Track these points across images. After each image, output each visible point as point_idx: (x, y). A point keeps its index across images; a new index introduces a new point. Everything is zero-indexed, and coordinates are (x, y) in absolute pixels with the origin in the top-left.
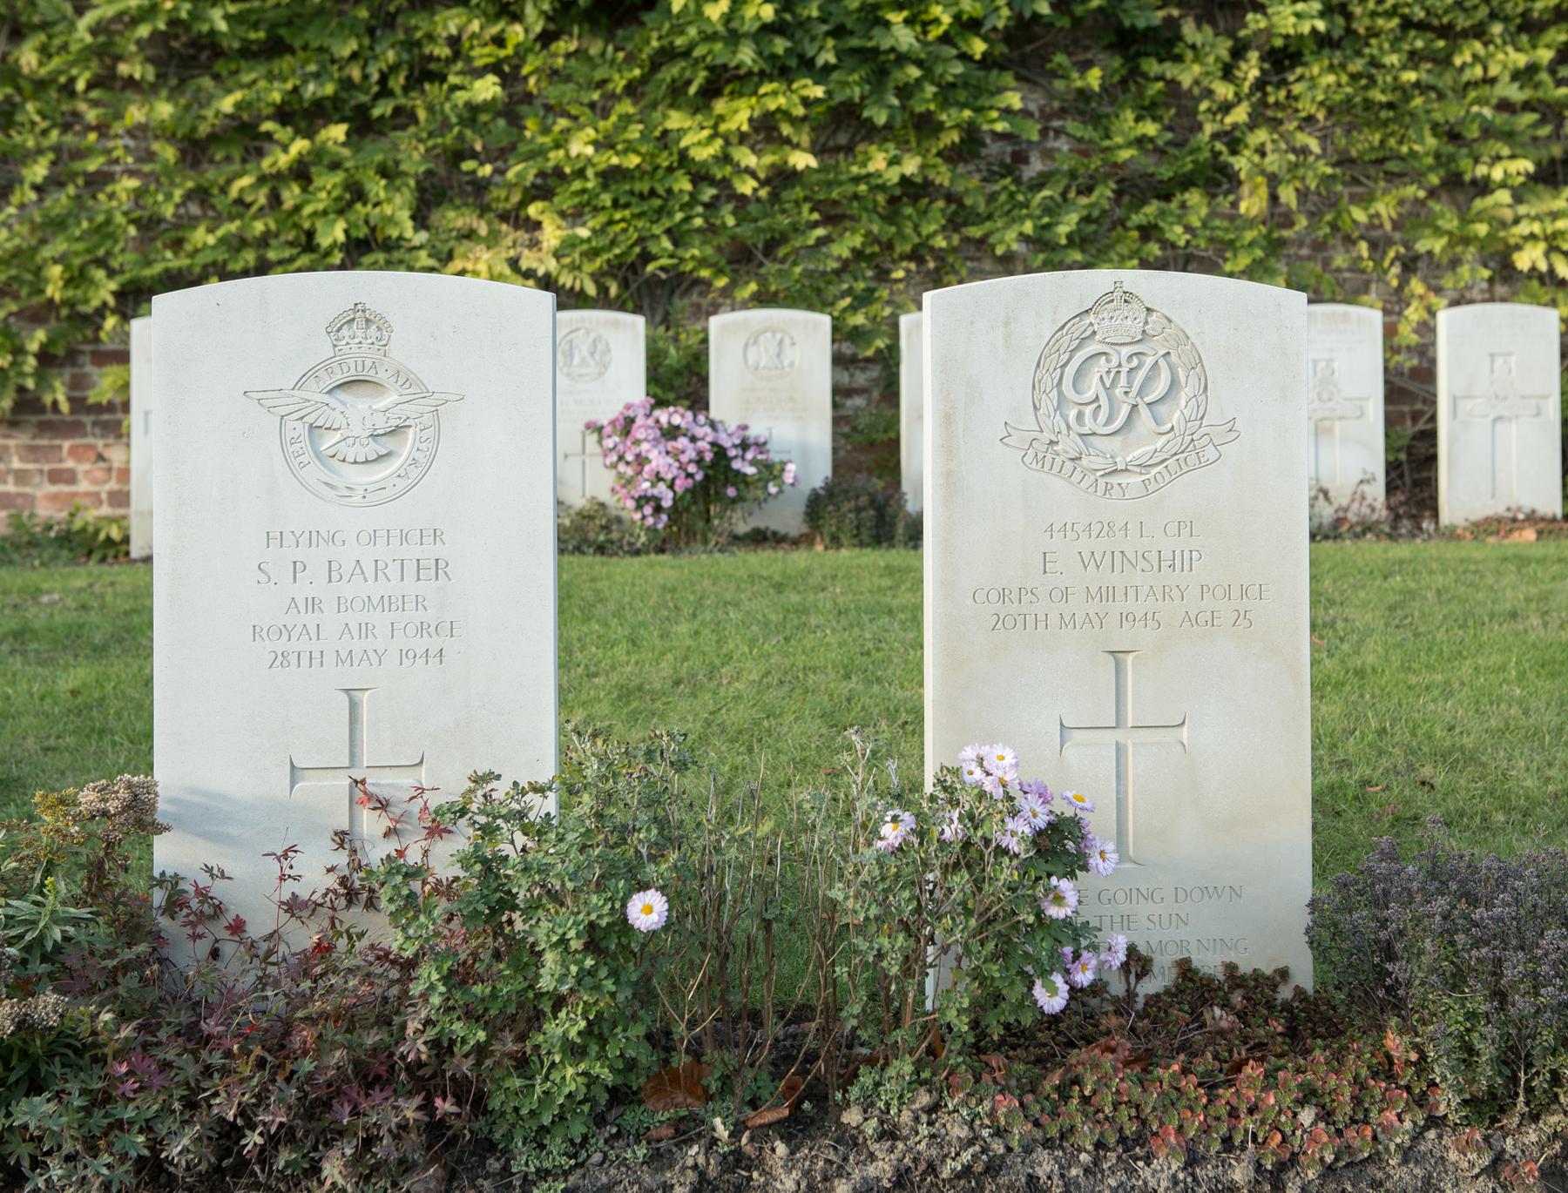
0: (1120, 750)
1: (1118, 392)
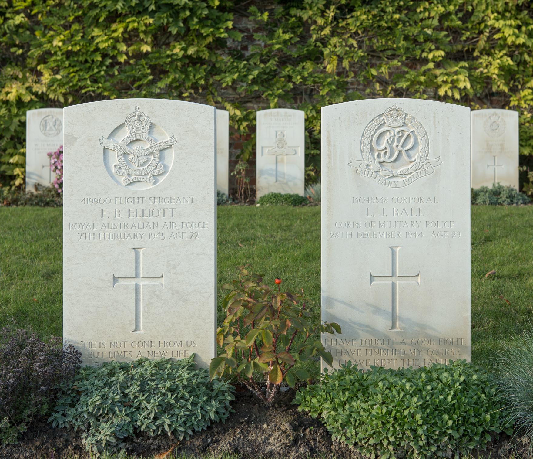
0: (393, 285)
1: (394, 145)
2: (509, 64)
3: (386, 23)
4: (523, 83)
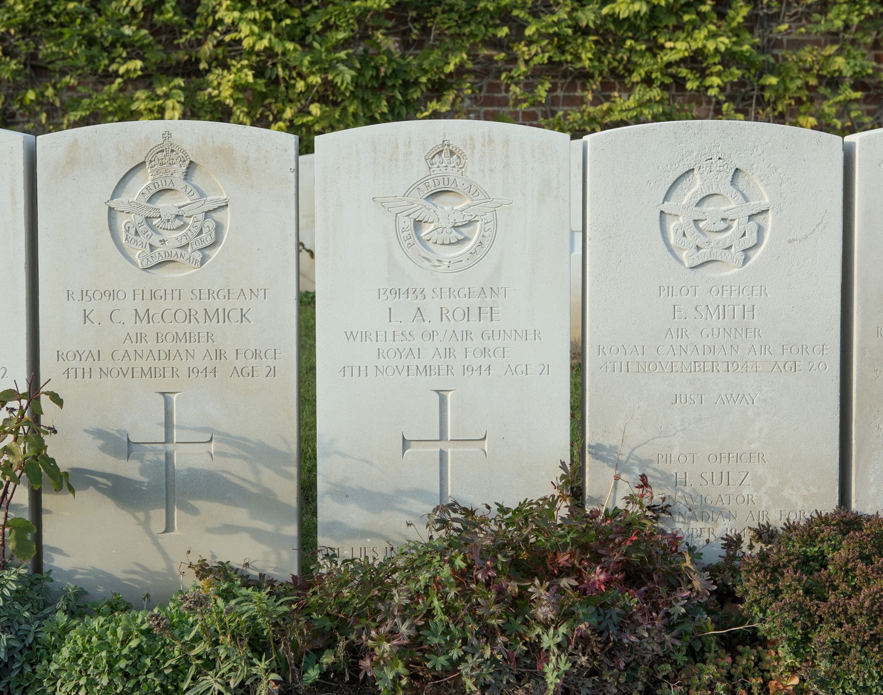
0: (443, 455)
3: (57, 16)
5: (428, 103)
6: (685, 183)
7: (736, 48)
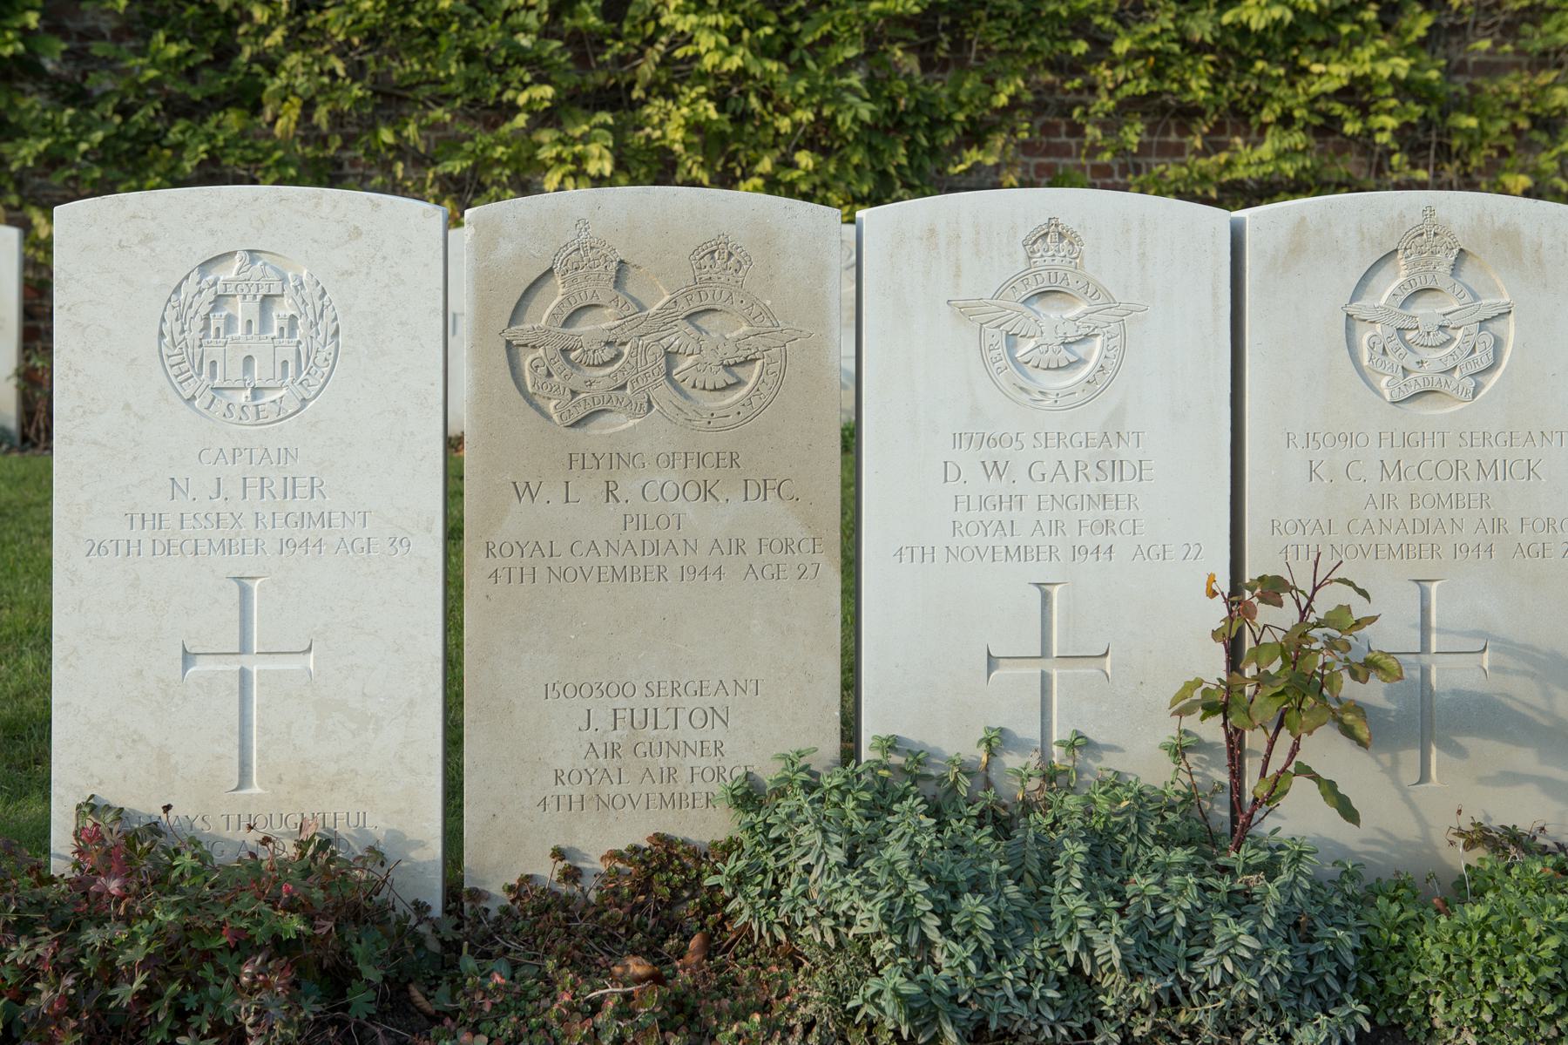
2: (708, 119)
3: (422, 18)
4: (748, 164)
5: (965, 152)
6: (1387, 270)
7: (1418, 75)
